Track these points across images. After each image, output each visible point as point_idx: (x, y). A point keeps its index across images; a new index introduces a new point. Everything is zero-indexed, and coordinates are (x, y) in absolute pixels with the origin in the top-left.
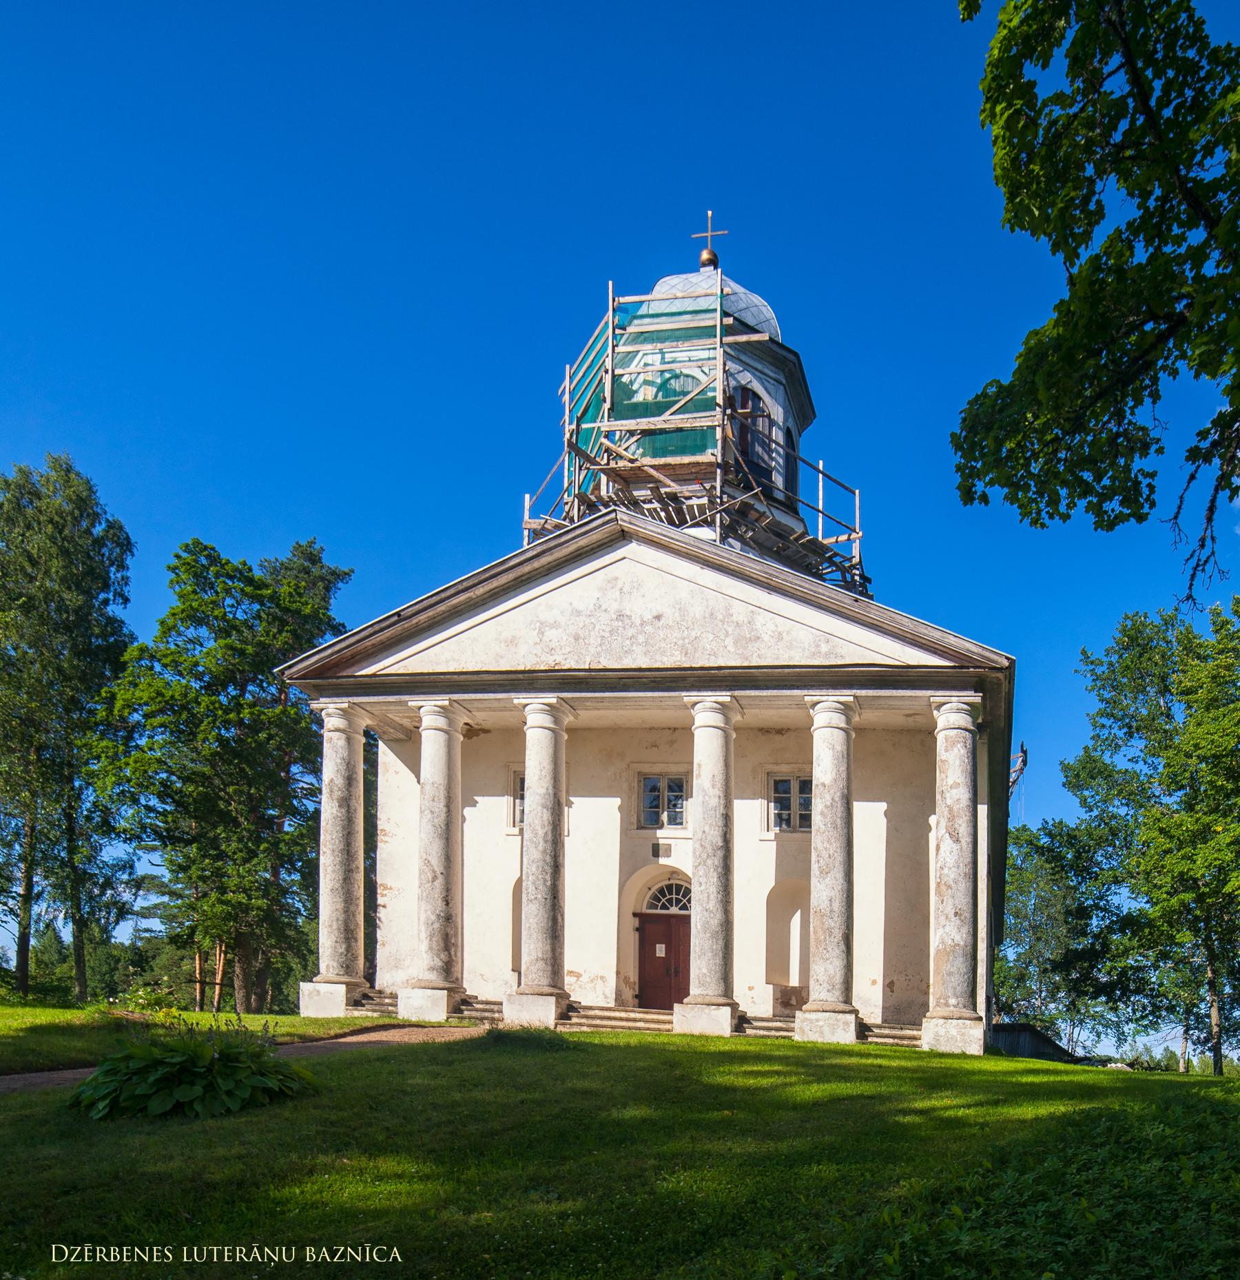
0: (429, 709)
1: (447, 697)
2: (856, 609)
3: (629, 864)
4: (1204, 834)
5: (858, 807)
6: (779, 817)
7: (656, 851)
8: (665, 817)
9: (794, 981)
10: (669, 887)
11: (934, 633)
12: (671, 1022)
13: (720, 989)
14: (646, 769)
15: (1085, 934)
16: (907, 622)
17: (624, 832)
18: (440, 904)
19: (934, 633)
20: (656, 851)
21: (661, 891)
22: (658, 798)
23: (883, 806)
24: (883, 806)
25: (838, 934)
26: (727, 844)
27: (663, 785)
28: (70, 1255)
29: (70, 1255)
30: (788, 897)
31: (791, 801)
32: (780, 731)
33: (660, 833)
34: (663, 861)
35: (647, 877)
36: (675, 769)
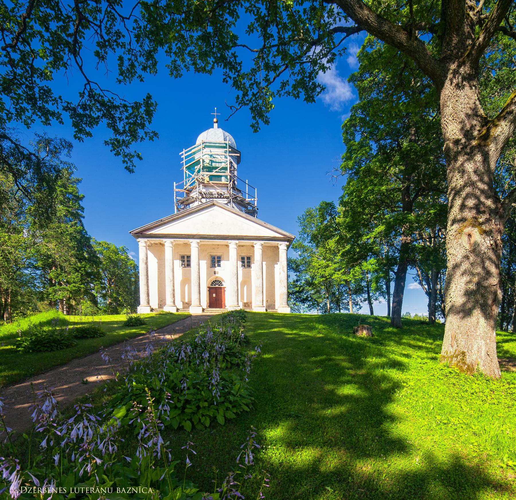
0: (168, 243)
1: (173, 239)
2: (265, 225)
3: (208, 275)
4: (328, 266)
5: (200, 261)
6: (182, 264)
7: (215, 273)
8: (216, 265)
9: (186, 301)
10: (220, 281)
11: (280, 231)
12: (497, 335)
13: (198, 303)
14: (212, 254)
15: (297, 287)
16: (275, 228)
17: (207, 269)
18: (172, 287)
19: (280, 231)
20: (215, 273)
21: (214, 281)
22: (215, 261)
23: (205, 261)
24: (205, 261)
25: (261, 291)
26: (228, 271)
27: (216, 258)
28: (28, 491)
29: (28, 491)
30: (186, 280)
31: (186, 261)
32: (242, 246)
33: (216, 269)
34: (216, 275)
35: (213, 278)
36: (188, 254)
